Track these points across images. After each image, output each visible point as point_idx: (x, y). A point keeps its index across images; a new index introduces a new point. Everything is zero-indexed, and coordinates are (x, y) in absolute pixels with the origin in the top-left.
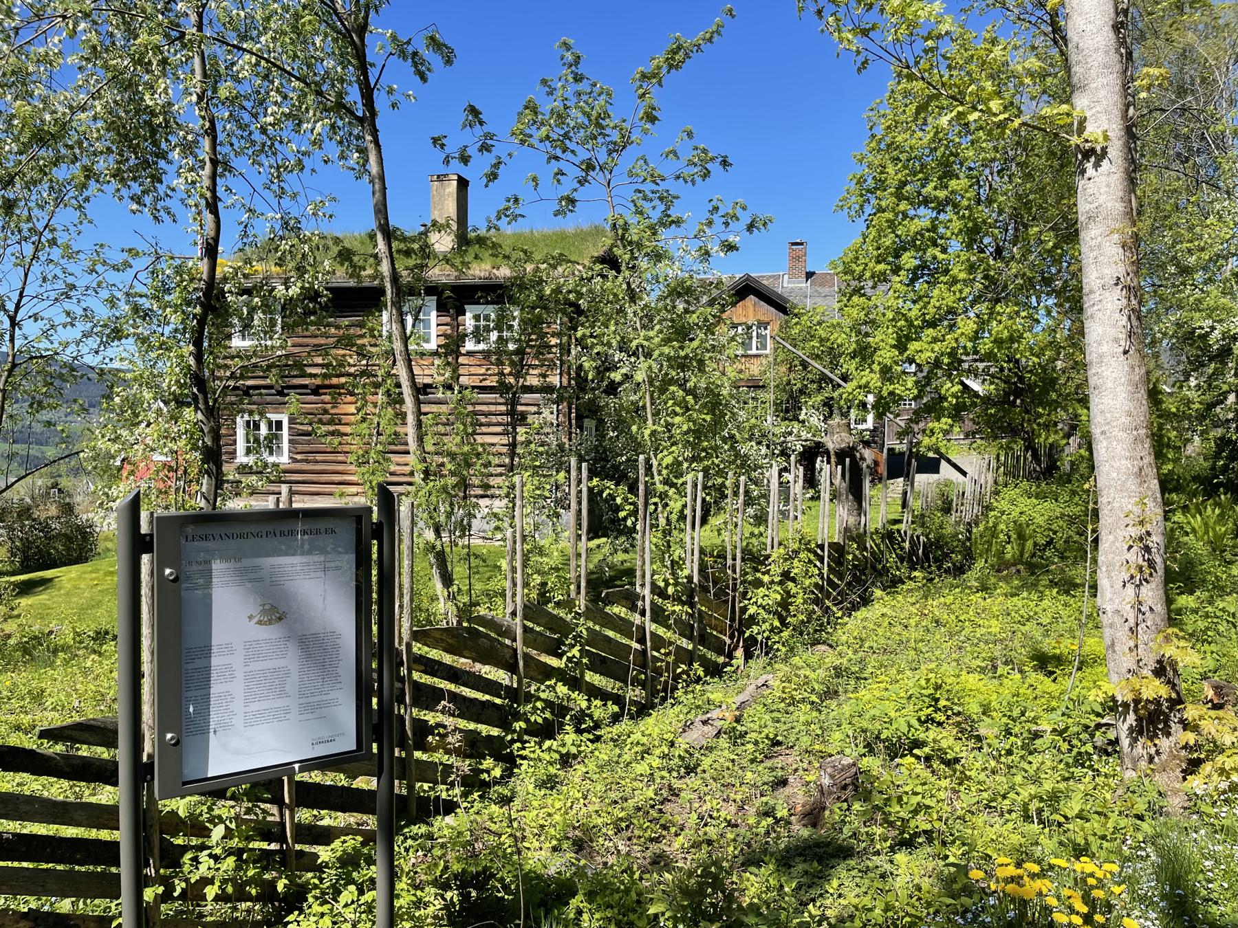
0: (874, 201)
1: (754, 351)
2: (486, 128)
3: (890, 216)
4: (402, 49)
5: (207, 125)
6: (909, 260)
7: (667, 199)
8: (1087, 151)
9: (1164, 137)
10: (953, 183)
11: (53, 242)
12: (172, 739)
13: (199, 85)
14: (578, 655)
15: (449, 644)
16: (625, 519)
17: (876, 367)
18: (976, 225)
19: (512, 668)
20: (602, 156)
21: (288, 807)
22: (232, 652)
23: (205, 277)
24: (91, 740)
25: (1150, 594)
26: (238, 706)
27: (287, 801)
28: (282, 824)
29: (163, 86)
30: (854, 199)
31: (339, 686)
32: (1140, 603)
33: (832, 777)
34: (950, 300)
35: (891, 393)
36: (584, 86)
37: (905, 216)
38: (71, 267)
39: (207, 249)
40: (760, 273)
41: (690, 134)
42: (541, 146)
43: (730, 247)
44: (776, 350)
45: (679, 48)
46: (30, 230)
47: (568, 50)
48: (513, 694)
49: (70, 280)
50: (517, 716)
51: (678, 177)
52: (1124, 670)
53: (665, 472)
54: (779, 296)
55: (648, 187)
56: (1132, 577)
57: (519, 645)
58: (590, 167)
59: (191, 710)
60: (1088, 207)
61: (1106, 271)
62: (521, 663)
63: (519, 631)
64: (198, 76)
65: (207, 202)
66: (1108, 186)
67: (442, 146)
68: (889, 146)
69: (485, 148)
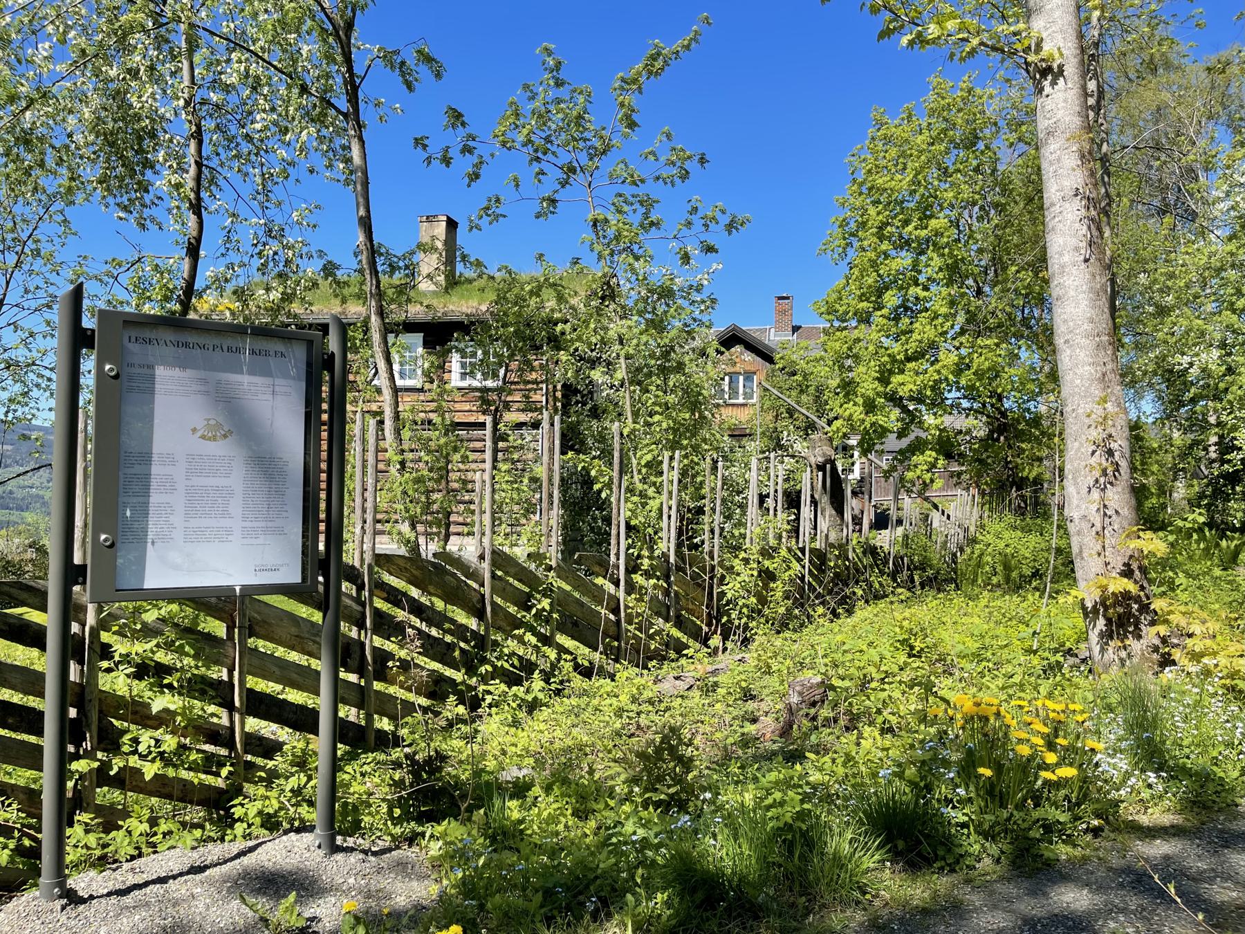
0: (856, 244)
1: (741, 400)
2: (468, 130)
3: (873, 255)
4: (389, 58)
5: (194, 128)
6: (891, 299)
7: (647, 203)
8: (1045, 69)
9: (1140, 183)
10: (933, 223)
11: (37, 253)
12: (106, 540)
13: (186, 90)
14: (548, 608)
15: (414, 576)
16: (600, 491)
17: (860, 400)
18: (956, 262)
19: (480, 614)
20: (584, 159)
21: (238, 710)
22: (173, 463)
23: (186, 275)
24: (30, 601)
25: (1116, 497)
26: (177, 520)
27: (237, 704)
28: (232, 729)
29: (150, 90)
30: (837, 243)
31: (285, 514)
32: (1105, 506)
33: (800, 694)
34: (930, 333)
35: (873, 424)
36: (563, 92)
37: (887, 256)
38: (53, 278)
39: (188, 249)
40: (749, 327)
41: (668, 136)
42: (524, 150)
43: (710, 249)
44: (762, 397)
45: (659, 54)
46: (13, 240)
47: (549, 55)
48: (482, 642)
49: (51, 290)
50: (484, 661)
51: (658, 178)
52: (1092, 576)
53: (644, 470)
54: (767, 346)
55: (628, 190)
56: (1097, 481)
57: (487, 590)
58: (573, 170)
59: (128, 513)
60: (1046, 123)
61: (1066, 183)
62: (489, 609)
63: (487, 576)
64: (186, 83)
65: (191, 203)
66: (1065, 101)
67: (424, 147)
68: (870, 189)
69: (467, 150)
